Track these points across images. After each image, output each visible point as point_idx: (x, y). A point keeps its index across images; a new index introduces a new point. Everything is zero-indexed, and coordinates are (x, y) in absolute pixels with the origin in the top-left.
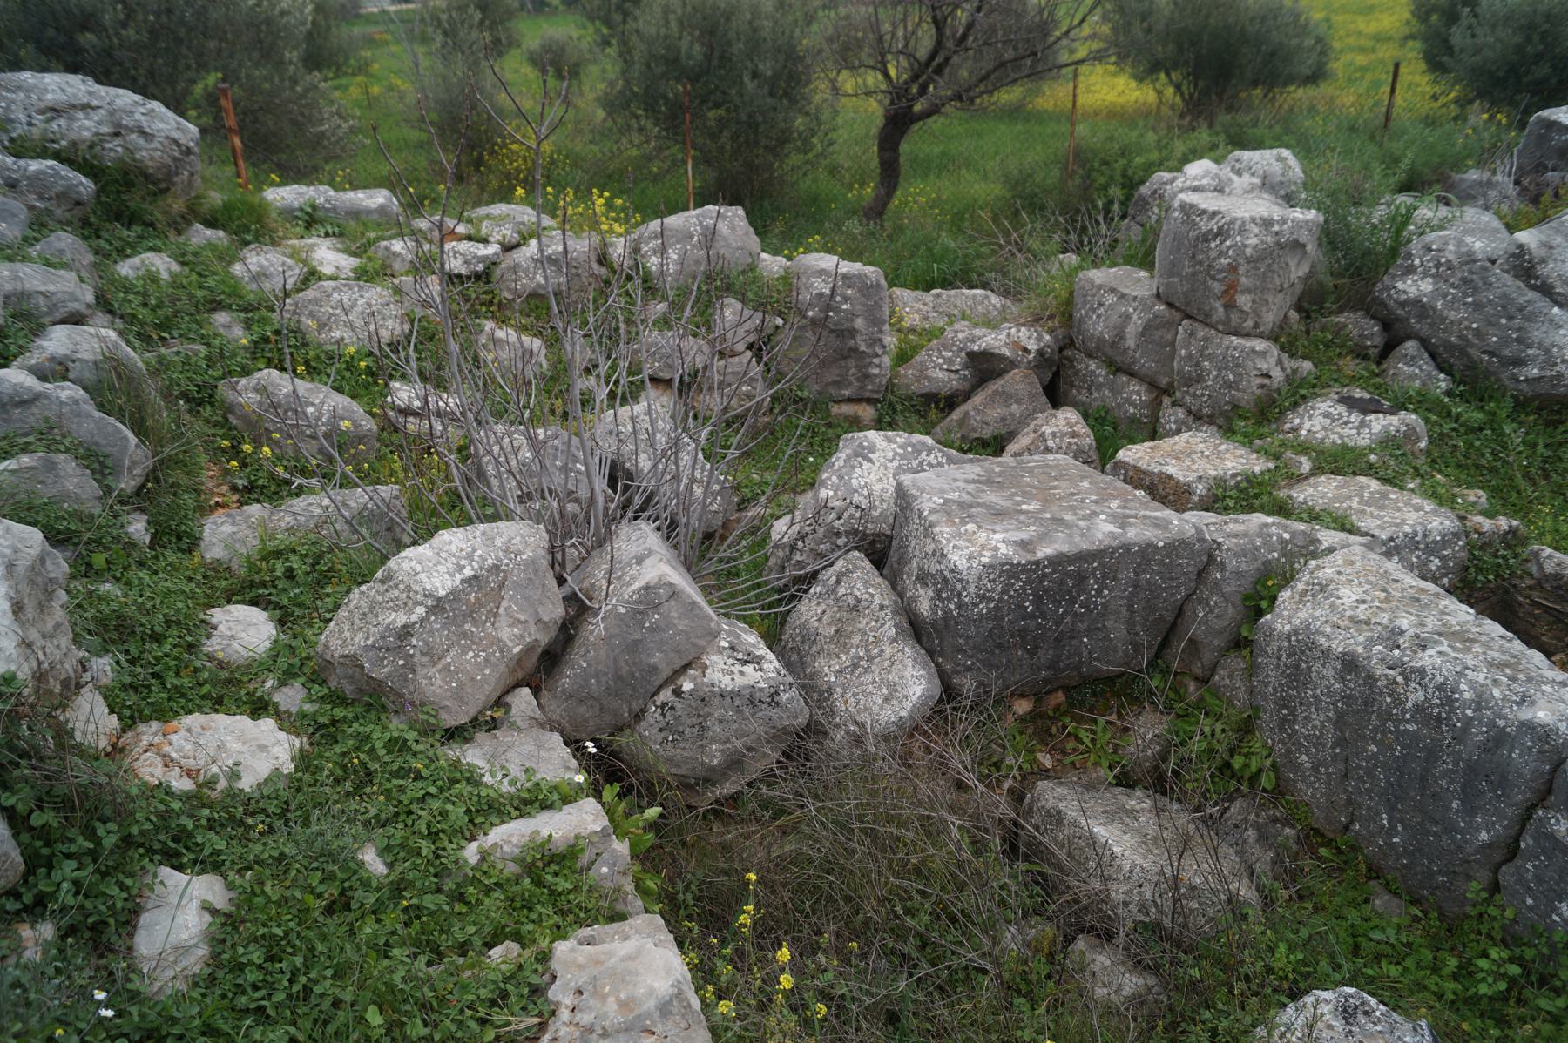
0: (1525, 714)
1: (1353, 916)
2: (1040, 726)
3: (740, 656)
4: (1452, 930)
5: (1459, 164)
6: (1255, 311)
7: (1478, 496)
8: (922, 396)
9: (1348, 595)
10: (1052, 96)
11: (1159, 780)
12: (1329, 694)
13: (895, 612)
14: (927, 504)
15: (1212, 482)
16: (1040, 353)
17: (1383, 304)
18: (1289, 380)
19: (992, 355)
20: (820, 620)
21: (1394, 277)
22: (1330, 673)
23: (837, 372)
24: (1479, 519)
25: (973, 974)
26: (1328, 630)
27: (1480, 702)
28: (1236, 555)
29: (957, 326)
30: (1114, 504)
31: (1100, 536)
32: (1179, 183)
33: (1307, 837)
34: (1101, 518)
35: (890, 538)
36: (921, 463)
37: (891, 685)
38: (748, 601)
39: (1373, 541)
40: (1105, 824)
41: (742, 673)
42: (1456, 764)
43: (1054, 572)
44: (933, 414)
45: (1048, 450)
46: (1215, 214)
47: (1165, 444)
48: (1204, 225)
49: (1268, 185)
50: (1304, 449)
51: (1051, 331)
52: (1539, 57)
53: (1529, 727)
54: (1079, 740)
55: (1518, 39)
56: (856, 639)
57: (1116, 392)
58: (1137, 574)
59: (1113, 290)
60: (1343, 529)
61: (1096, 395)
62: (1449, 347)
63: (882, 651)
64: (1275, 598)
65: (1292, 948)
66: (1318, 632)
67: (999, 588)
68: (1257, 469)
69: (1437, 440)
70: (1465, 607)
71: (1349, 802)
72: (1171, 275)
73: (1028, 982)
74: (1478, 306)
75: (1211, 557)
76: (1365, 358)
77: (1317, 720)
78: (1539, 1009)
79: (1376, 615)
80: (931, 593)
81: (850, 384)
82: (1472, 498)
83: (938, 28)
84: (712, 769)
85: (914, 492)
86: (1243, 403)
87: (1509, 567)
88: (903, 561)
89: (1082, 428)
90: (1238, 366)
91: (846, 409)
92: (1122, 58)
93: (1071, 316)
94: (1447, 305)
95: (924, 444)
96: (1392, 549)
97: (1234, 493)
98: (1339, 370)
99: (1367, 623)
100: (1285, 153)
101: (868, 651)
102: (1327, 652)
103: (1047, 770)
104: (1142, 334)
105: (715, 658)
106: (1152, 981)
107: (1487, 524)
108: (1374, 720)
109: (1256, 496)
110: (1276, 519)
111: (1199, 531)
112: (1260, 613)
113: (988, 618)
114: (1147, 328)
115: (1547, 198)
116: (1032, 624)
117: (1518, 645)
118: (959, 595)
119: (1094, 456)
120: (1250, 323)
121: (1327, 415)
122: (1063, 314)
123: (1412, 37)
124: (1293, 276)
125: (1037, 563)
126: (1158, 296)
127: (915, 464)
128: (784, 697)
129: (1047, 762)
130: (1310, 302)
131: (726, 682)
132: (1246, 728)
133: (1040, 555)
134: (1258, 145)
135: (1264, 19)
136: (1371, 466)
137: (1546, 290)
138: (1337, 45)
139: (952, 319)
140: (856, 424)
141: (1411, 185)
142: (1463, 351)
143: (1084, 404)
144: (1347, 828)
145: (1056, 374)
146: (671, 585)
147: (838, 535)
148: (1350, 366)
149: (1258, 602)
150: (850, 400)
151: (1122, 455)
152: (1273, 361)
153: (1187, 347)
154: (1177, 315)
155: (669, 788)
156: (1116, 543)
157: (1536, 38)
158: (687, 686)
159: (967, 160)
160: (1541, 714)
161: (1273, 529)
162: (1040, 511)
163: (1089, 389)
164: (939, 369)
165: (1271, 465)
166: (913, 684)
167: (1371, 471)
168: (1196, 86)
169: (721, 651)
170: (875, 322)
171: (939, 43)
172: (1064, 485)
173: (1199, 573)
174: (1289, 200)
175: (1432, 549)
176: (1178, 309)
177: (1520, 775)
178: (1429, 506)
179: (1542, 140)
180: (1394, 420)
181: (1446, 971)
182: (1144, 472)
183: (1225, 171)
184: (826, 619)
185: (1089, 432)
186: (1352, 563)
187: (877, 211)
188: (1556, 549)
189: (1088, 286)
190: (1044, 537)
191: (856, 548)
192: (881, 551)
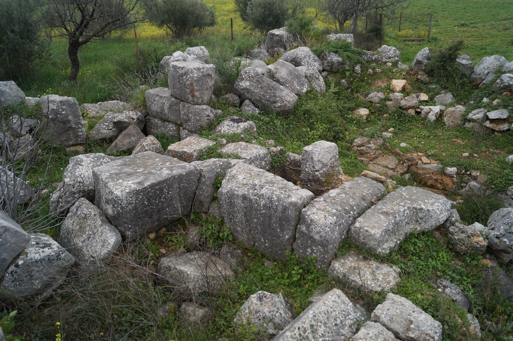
0: (290, 200)
1: (260, 270)
2: (159, 240)
3: (41, 246)
4: (284, 265)
5: (252, 47)
6: (201, 97)
7: (272, 142)
8: (100, 139)
9: (240, 177)
10: (130, 35)
11: (200, 247)
12: (241, 208)
13: (100, 216)
14: (104, 176)
15: (198, 151)
16: (138, 119)
17: (237, 90)
18: (215, 116)
19: (121, 122)
20: (73, 225)
21: (238, 82)
22: (240, 201)
23: (66, 136)
24: (273, 148)
25: (150, 328)
26: (237, 189)
27: (279, 200)
28: (208, 172)
29: (108, 114)
30: (168, 164)
31: (164, 175)
32: (172, 59)
33: (244, 251)
34: (165, 169)
35: (94, 191)
36: (101, 163)
37: (104, 241)
38: (44, 224)
39: (246, 160)
40: (184, 266)
41: (43, 252)
42: (276, 219)
43: (152, 190)
44: (105, 145)
45: (146, 150)
46: (183, 68)
47: (182, 142)
48: (180, 72)
49: (199, 58)
50: (223, 136)
51: (141, 111)
52: (269, 15)
53: (291, 203)
54: (173, 241)
55: (263, 10)
56: (88, 229)
57: (165, 128)
58: (179, 185)
59: (157, 95)
60: (237, 158)
61: (159, 130)
62: (256, 100)
63: (98, 230)
64: (221, 183)
65: (244, 286)
66: (234, 190)
67: (134, 199)
68: (211, 145)
69: (259, 127)
70: (271, 174)
71: (253, 237)
72: (174, 88)
73: (169, 324)
74: (262, 88)
75: (201, 174)
76: (236, 107)
77: (240, 216)
78: (308, 279)
79: (249, 182)
80: (111, 206)
81: (72, 139)
82: (270, 143)
83: (81, 12)
84: (38, 290)
85: (99, 173)
86: (203, 126)
87: (282, 160)
88: (100, 198)
89: (156, 141)
90: (199, 114)
91: (72, 149)
92: (151, 20)
93: (146, 105)
94: (255, 88)
95: (101, 156)
96: (251, 161)
97: (205, 153)
98: (229, 111)
99: (247, 184)
100: (203, 47)
101: (93, 231)
102: (238, 195)
103: (164, 254)
104: (169, 108)
105: (30, 249)
106: (207, 309)
107: (275, 149)
108: (254, 212)
109: (212, 153)
110: (217, 159)
111: (195, 167)
112: (218, 188)
113: (133, 210)
114: (170, 106)
115: (275, 55)
116: (148, 208)
117: (285, 182)
118: (121, 204)
119: (162, 149)
120: (200, 101)
121: (228, 125)
122: (143, 105)
123: (236, 11)
124: (210, 85)
125: (145, 188)
126: (172, 95)
127: (99, 163)
128: (63, 256)
129: (164, 251)
130: (217, 92)
131: (37, 257)
132: (222, 223)
133: (146, 185)
134: (197, 45)
135: (193, 6)
136: (242, 138)
137: (278, 81)
138: (217, 14)
139: (107, 111)
140: (77, 153)
141: (240, 55)
142: (261, 102)
143: (156, 133)
144: (254, 245)
145: (145, 125)
146: (4, 227)
147: (75, 193)
148: (232, 109)
149: (217, 185)
150: (73, 145)
151: (170, 148)
152: (209, 111)
153: (183, 111)
154: (179, 101)
155: (21, 302)
156: (170, 176)
157: (267, 10)
158: (20, 262)
159: (103, 57)
160: (293, 199)
161: (217, 162)
162: (144, 171)
163: (157, 128)
164: (105, 130)
165: (215, 143)
166: (111, 238)
167: (242, 140)
168: (176, 28)
169: (33, 246)
170: (76, 116)
171: (83, 17)
172: (151, 161)
173: (198, 180)
174: (207, 62)
175: (262, 159)
176: (179, 99)
177: (292, 217)
178: (259, 147)
179: (272, 39)
180: (246, 124)
181: (285, 277)
182: (177, 152)
183: (185, 54)
184: (75, 224)
185: (159, 142)
186: (240, 168)
187: (73, 77)
188: (293, 153)
189: (149, 95)
190: (146, 179)
191: (83, 196)
192: (92, 196)
